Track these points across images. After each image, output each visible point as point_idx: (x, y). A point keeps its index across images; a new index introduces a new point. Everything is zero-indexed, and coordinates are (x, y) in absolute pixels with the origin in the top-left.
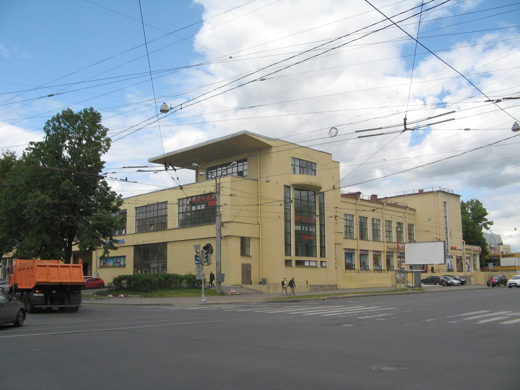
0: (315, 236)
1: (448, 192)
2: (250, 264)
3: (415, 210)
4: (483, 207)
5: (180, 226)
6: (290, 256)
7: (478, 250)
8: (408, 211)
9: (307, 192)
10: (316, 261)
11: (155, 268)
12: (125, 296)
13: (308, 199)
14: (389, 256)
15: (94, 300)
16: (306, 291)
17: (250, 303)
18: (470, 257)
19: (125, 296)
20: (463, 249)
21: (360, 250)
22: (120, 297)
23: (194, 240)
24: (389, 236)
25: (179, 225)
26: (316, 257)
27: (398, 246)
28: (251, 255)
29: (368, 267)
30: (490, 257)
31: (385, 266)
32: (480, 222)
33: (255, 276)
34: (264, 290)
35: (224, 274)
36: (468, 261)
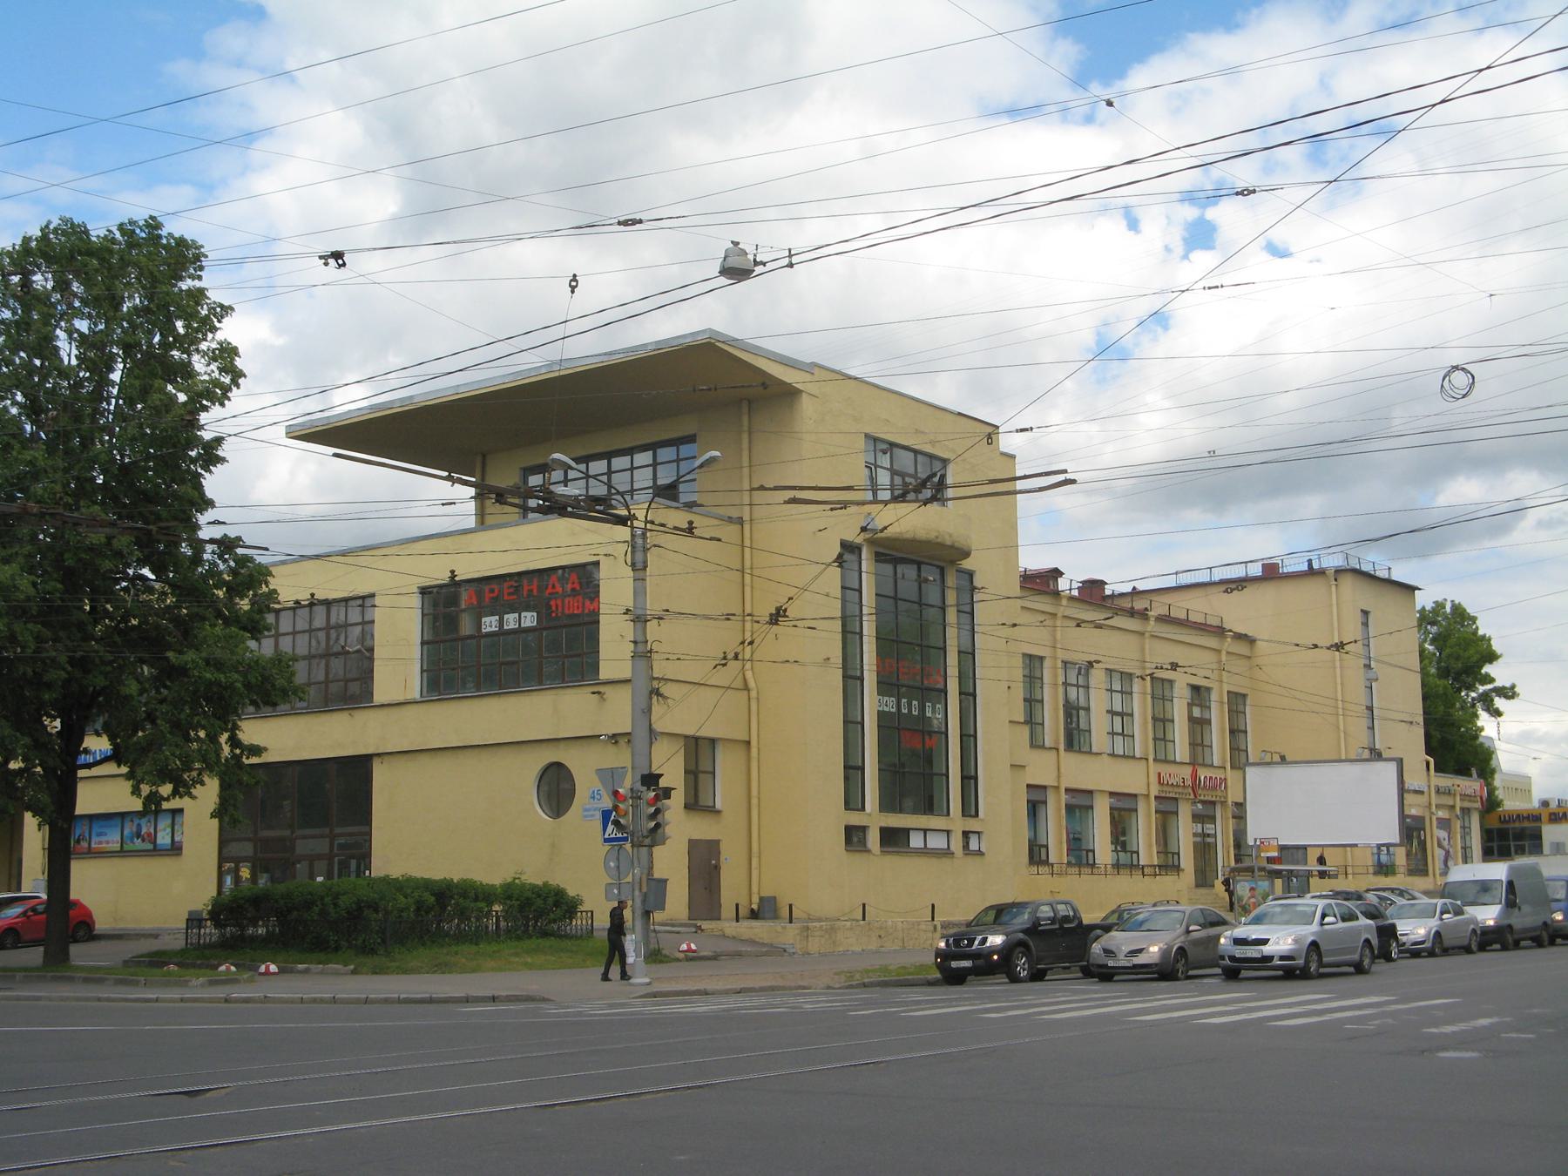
0: (943, 736)
1: (1373, 573)
2: (717, 842)
3: (1249, 640)
4: (1481, 632)
5: (428, 692)
6: (858, 810)
7: (1478, 793)
8: (1229, 644)
9: (915, 566)
10: (948, 832)
11: (320, 857)
12: (282, 971)
13: (896, 592)
14: (1120, 809)
15: (202, 985)
16: (931, 945)
17: (804, 988)
18: (1449, 819)
19: (282, 971)
20: (1426, 790)
21: (1067, 790)
22: (261, 974)
23: (439, 753)
24: (1122, 734)
25: (425, 690)
26: (948, 814)
27: (1194, 776)
28: (718, 806)
29: (1090, 854)
30: (1505, 822)
31: (1061, 850)
32: (1471, 687)
33: (732, 889)
34: (791, 942)
35: (665, 881)
36: (1443, 834)
